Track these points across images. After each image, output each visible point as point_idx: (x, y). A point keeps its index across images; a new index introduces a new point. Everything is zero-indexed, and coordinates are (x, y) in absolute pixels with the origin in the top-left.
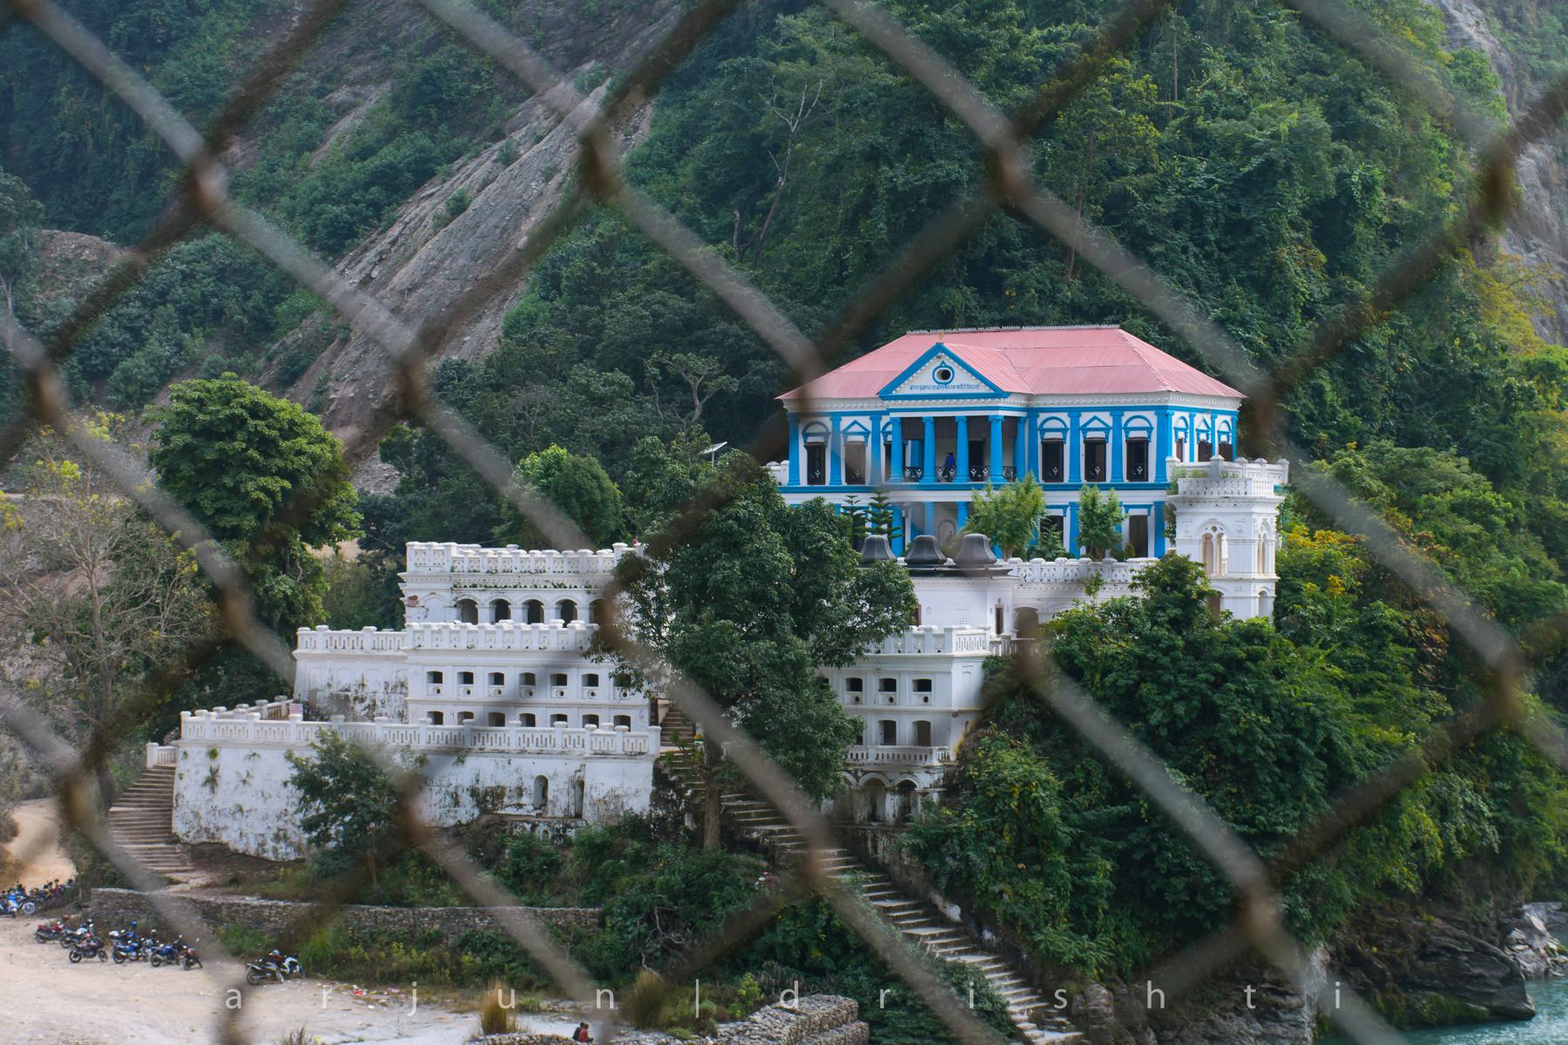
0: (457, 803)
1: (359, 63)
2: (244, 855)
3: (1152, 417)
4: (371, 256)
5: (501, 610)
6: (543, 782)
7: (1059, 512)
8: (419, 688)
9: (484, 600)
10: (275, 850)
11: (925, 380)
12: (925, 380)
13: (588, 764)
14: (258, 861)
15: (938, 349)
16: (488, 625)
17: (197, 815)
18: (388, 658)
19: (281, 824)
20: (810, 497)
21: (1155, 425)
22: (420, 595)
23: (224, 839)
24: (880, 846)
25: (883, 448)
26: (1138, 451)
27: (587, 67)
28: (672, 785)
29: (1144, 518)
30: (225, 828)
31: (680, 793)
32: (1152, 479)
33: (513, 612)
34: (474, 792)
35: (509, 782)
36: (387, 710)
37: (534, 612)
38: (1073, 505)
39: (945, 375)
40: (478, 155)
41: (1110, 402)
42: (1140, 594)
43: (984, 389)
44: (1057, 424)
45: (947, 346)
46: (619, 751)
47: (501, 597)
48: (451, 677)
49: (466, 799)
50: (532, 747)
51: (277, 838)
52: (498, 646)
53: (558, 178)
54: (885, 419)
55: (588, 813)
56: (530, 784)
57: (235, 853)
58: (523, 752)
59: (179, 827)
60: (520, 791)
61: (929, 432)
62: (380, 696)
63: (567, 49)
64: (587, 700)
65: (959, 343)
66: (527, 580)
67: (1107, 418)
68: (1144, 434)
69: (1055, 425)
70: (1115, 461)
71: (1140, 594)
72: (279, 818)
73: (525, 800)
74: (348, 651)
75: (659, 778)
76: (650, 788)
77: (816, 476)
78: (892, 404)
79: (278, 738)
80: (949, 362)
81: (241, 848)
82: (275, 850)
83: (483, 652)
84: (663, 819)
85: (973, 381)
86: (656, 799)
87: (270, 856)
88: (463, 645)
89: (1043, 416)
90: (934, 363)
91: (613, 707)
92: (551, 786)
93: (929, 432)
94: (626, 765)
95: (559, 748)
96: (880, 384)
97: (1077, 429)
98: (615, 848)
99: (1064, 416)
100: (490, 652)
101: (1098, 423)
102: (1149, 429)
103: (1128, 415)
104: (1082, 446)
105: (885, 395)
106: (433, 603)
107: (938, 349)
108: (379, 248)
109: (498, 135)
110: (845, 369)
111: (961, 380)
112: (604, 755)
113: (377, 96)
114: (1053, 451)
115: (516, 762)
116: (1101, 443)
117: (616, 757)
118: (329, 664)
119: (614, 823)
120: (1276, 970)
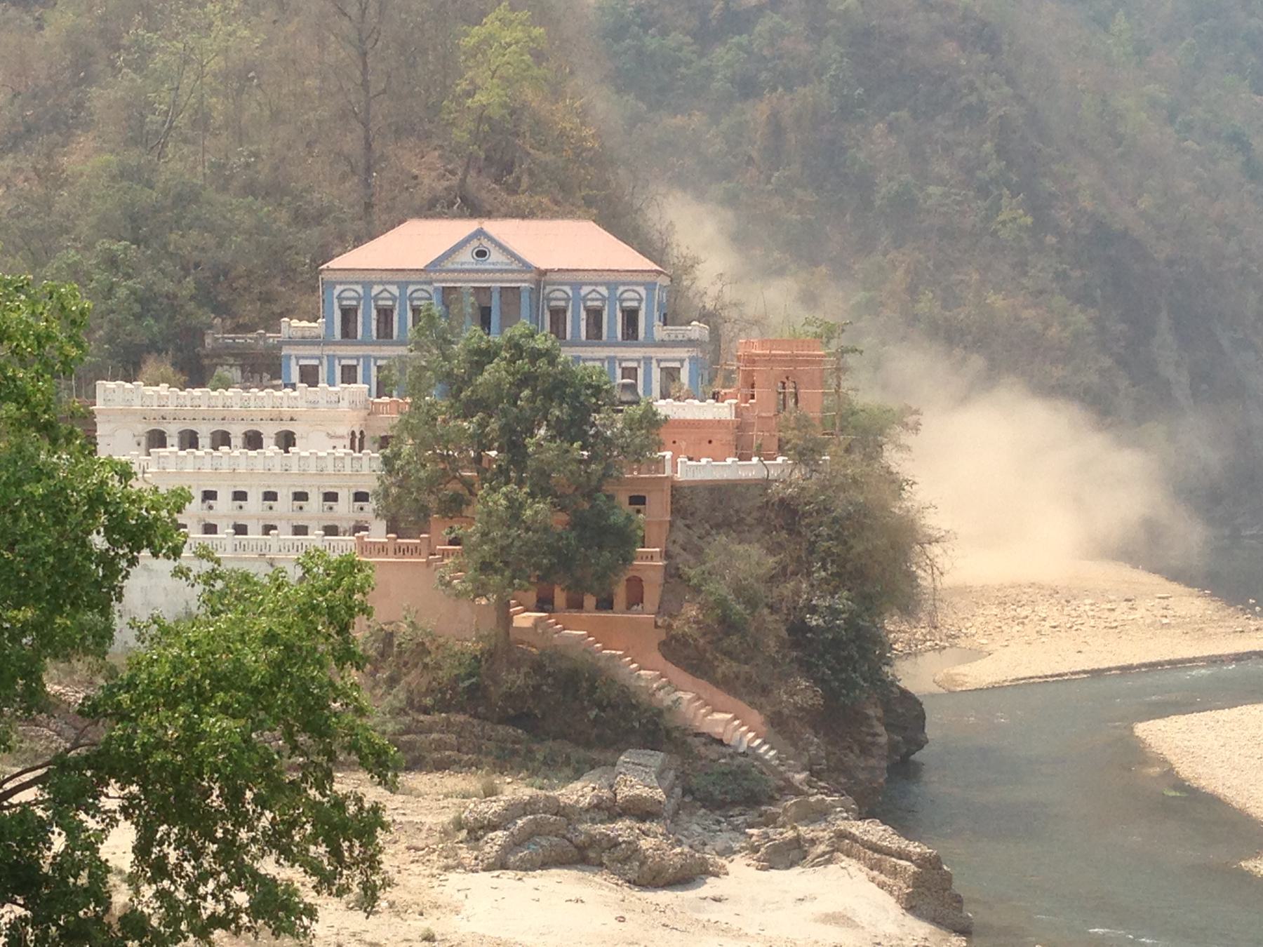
3: (642, 290)
5: (222, 439)
7: (354, 362)
12: (466, 258)
15: (480, 233)
21: (644, 296)
25: (410, 314)
29: (355, 367)
32: (605, 337)
39: (481, 254)
41: (400, 277)
43: (514, 267)
44: (353, 294)
45: (485, 229)
47: (255, 428)
48: (285, 496)
61: (496, 296)
65: (497, 228)
67: (394, 290)
68: (635, 304)
69: (559, 295)
70: (613, 324)
77: (348, 331)
90: (475, 243)
91: (320, 519)
99: (359, 288)
101: (595, 295)
102: (640, 300)
103: (621, 289)
104: (583, 315)
111: (495, 257)
120: (677, 728)
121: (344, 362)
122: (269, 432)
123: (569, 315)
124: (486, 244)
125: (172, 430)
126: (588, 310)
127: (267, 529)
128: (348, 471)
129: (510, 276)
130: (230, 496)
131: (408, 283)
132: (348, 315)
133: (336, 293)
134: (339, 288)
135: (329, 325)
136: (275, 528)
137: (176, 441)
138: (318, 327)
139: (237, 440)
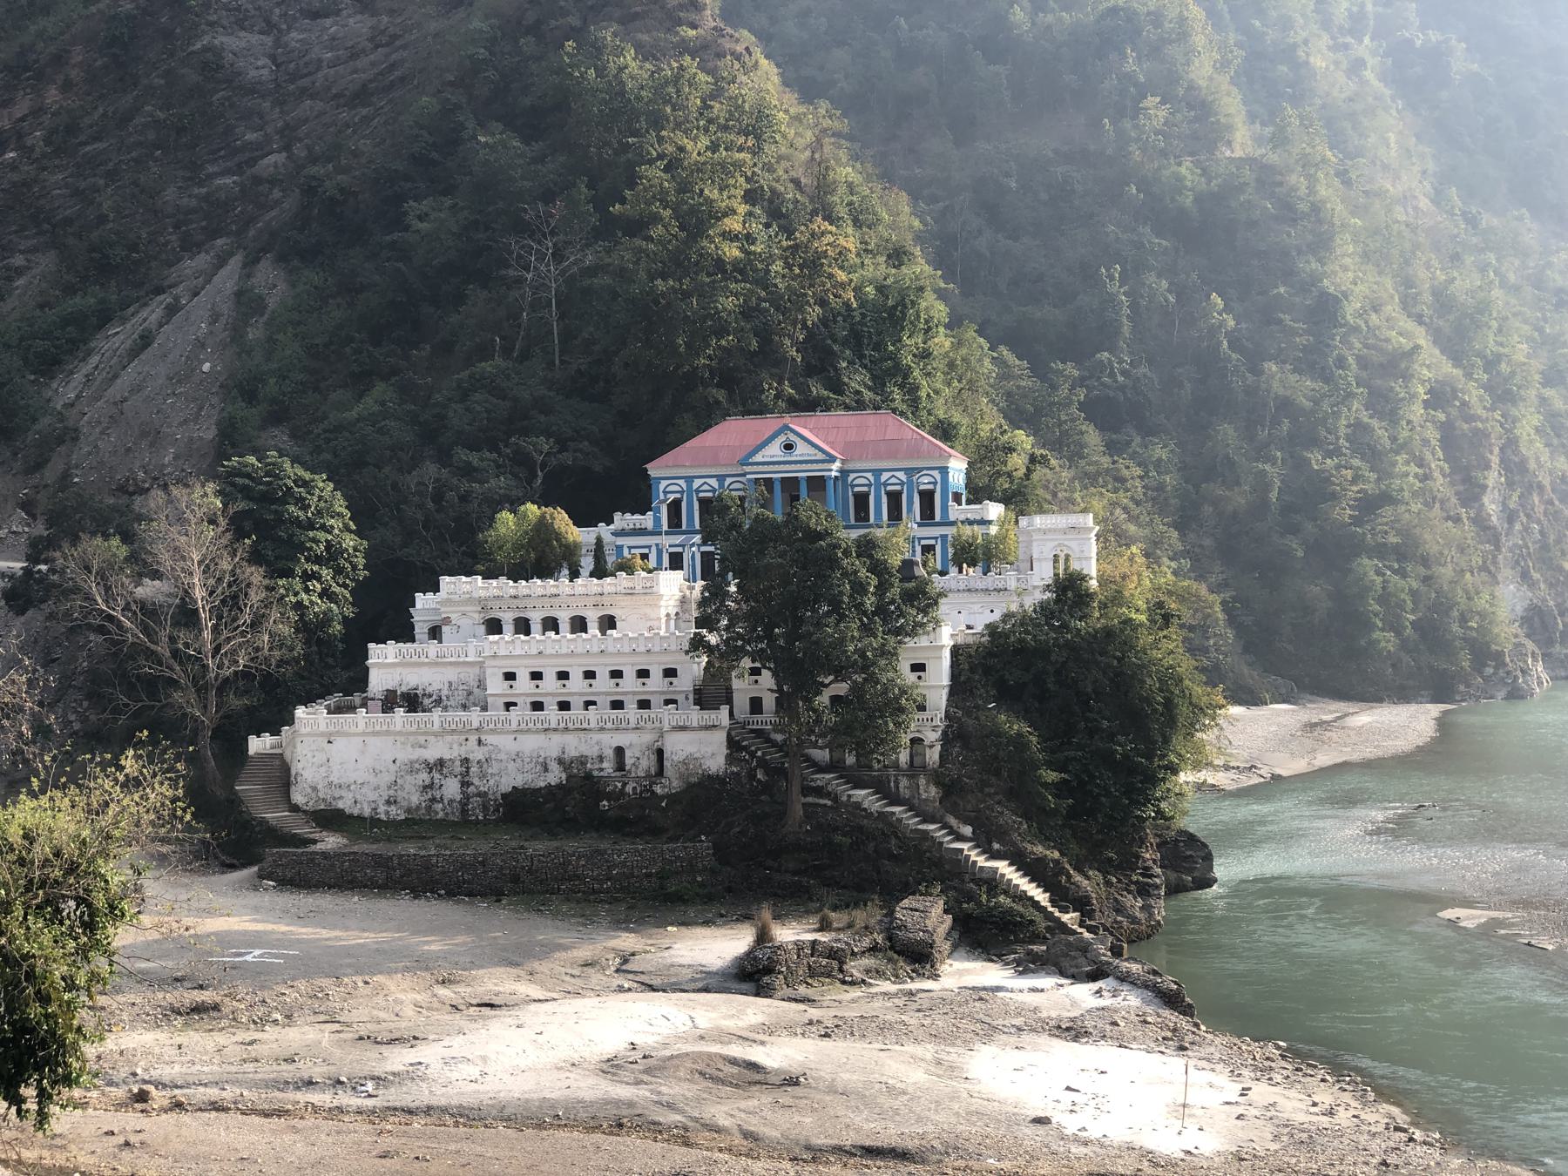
0: (546, 770)
1: (27, 237)
2: (360, 818)
3: (936, 474)
4: (78, 377)
6: (620, 751)
7: (932, 542)
8: (496, 686)
9: (507, 618)
10: (387, 813)
11: (774, 451)
13: (666, 736)
14: (374, 822)
16: (538, 637)
17: (315, 789)
18: (451, 664)
19: (392, 792)
20: (862, 532)
22: (453, 616)
23: (340, 805)
24: (901, 785)
26: (927, 497)
27: (219, 242)
28: (745, 748)
30: (341, 798)
31: (752, 754)
32: (938, 518)
33: (533, 627)
34: (560, 761)
35: (592, 751)
36: (452, 703)
37: (579, 625)
38: (944, 537)
39: (789, 447)
40: (146, 305)
42: (1048, 595)
43: (820, 456)
46: (695, 724)
49: (554, 766)
50: (609, 725)
51: (388, 802)
52: (564, 651)
53: (223, 320)
54: (729, 480)
55: (669, 769)
56: (609, 753)
57: (351, 816)
58: (602, 729)
59: (298, 798)
60: (601, 759)
61: (777, 488)
62: (445, 692)
63: (203, 228)
64: (510, 692)
66: (547, 602)
67: (902, 476)
68: (865, 489)
71: (1048, 595)
72: (389, 788)
73: (605, 765)
74: (415, 659)
75: (732, 744)
76: (725, 751)
78: (748, 469)
79: (385, 728)
80: (792, 437)
81: (356, 812)
82: (387, 813)
83: (552, 656)
84: (738, 774)
85: (813, 451)
86: (730, 759)
87: (383, 817)
88: (535, 652)
89: (852, 476)
90: (782, 439)
92: (628, 754)
93: (777, 488)
94: (703, 734)
95: (632, 725)
96: (740, 455)
97: (878, 484)
98: (703, 796)
100: (557, 655)
102: (935, 483)
104: (884, 499)
105: (744, 462)
106: (464, 622)
107: (786, 428)
108: (84, 371)
109: (159, 291)
110: (688, 444)
111: (802, 450)
112: (683, 728)
113: (46, 262)
114: (862, 500)
115: (596, 737)
116: (899, 493)
117: (694, 729)
118: (399, 670)
119: (694, 780)
121: (924, 542)
122: (592, 617)
123: (872, 498)
124: (792, 437)
125: (507, 618)
126: (889, 494)
127: (508, 706)
128: (657, 649)
129: (815, 466)
130: (528, 676)
131: (881, 471)
132: (675, 508)
133: (662, 487)
134: (664, 483)
135: (657, 520)
136: (515, 704)
137: (512, 628)
138: (647, 520)
139: (564, 626)
